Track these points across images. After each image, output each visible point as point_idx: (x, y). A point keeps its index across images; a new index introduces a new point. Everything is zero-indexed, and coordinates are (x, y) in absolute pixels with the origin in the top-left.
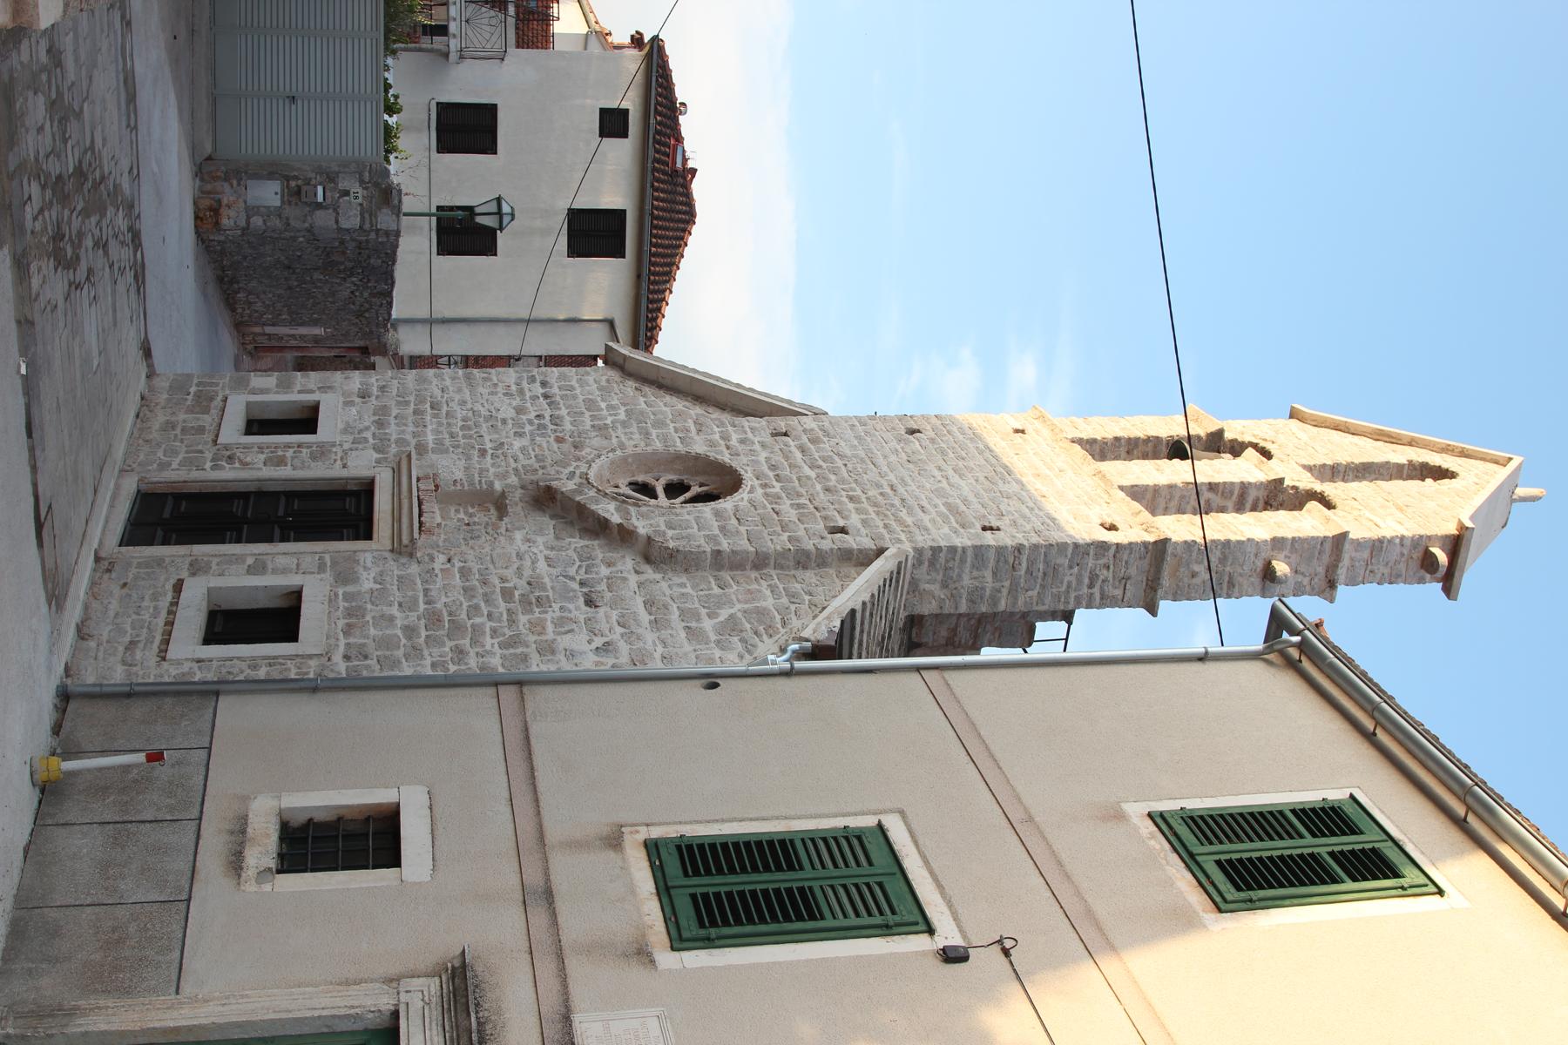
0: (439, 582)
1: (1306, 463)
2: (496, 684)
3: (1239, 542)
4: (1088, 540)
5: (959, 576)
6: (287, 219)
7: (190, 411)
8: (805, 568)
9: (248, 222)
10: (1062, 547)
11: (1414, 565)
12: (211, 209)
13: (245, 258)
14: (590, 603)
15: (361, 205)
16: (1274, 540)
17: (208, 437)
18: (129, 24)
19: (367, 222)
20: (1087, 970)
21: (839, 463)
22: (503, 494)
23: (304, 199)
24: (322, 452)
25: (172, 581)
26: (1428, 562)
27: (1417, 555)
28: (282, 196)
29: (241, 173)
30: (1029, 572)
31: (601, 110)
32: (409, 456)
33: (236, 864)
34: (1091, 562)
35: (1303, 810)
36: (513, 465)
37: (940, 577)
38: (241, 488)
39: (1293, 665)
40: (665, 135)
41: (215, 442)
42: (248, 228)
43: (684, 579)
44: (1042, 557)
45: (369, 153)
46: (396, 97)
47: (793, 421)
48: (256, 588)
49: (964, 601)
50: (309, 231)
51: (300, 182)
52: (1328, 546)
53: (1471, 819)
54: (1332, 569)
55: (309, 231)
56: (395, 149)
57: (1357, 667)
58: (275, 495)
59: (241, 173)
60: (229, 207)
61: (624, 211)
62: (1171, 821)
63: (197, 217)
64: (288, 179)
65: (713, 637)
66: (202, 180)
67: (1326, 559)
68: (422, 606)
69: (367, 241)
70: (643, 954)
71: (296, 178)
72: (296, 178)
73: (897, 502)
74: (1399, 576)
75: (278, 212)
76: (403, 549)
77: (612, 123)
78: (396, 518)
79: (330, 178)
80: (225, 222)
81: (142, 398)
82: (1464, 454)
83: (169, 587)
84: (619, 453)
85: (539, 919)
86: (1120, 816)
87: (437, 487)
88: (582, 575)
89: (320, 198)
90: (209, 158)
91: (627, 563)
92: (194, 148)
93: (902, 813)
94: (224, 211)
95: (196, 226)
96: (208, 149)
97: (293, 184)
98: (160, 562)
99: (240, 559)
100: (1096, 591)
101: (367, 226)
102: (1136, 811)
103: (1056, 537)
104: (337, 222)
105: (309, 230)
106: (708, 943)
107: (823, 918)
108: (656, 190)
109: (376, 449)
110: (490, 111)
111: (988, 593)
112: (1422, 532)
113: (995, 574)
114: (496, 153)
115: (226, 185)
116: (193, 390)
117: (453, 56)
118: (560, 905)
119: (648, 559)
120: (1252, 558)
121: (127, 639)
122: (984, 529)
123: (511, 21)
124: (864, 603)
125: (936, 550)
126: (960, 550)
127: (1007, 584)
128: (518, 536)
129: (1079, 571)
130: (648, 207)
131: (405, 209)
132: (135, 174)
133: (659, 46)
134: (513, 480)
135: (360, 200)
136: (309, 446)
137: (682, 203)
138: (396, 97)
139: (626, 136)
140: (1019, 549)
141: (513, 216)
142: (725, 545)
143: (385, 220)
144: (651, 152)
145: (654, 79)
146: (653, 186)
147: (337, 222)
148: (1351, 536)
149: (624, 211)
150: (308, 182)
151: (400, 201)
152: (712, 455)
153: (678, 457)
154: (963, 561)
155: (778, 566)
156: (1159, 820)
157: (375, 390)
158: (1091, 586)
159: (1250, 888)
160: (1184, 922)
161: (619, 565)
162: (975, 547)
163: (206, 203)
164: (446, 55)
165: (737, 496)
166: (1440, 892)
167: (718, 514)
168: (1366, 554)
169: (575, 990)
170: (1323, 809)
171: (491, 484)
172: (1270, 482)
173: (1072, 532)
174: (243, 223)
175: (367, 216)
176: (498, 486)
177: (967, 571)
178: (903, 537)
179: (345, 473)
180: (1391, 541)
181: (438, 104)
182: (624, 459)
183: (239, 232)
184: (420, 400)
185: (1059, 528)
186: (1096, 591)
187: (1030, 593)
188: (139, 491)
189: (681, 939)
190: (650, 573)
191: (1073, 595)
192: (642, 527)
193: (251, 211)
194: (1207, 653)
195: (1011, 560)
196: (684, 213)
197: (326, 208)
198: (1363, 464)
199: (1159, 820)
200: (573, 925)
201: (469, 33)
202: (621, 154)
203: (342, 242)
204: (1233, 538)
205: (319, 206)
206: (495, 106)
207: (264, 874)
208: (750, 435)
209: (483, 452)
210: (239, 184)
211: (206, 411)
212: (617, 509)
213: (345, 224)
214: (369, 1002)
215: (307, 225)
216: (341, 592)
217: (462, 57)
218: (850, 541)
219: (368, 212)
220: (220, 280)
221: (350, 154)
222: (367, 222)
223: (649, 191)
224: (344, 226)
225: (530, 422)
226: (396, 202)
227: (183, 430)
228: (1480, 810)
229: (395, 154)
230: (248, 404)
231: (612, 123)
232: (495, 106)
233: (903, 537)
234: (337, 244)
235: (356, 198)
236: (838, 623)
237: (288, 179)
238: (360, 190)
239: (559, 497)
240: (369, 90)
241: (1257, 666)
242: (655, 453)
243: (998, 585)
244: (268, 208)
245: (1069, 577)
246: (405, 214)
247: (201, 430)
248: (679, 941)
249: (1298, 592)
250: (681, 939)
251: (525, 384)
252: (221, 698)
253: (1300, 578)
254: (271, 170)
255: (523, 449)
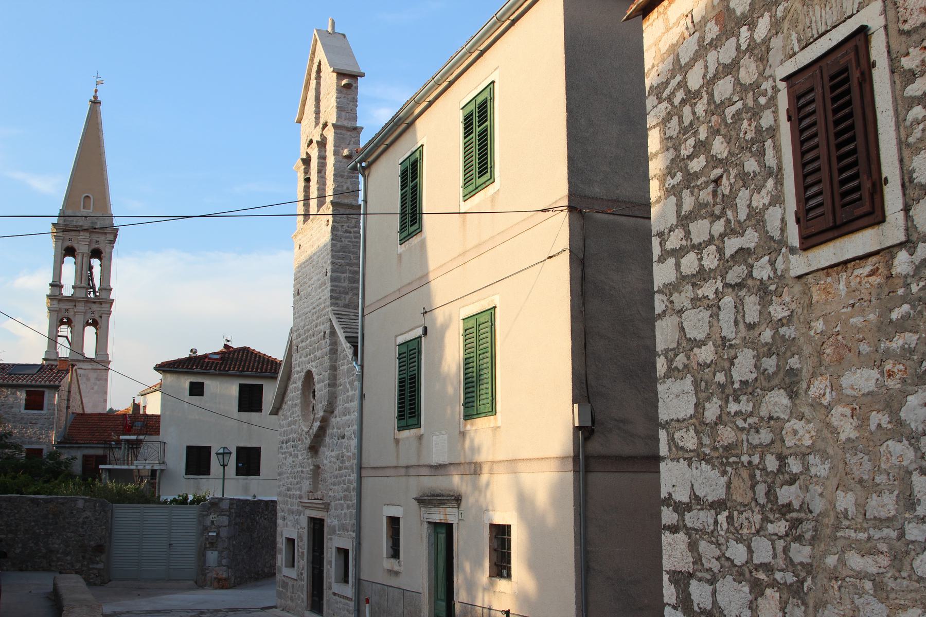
0: (336, 494)
1: (314, 126)
2: (361, 477)
3: (334, 170)
4: (330, 234)
5: (343, 287)
6: (223, 548)
7: (287, 591)
8: (337, 350)
9: (224, 566)
10: (333, 245)
11: (349, 91)
12: (219, 582)
13: (244, 568)
14: (343, 437)
15: (218, 516)
16: (334, 155)
17: (295, 583)
18: (128, 612)
19: (225, 513)
20: (432, 283)
21: (306, 328)
22: (314, 465)
23: (214, 541)
24: (300, 537)
25: (333, 595)
26: (348, 86)
27: (345, 91)
28: (213, 550)
29: (202, 568)
30: (343, 259)
31: (190, 395)
32: (301, 502)
33: (397, 573)
34: (340, 233)
35: (465, 133)
36: (306, 460)
37: (343, 296)
38: (311, 570)
39: (369, 166)
40: (203, 364)
41: (296, 580)
42: (227, 566)
43: (338, 399)
44: (337, 253)
45: (195, 512)
46: (179, 496)
47: (294, 342)
48: (335, 564)
49: (354, 285)
50: (230, 539)
51: (207, 543)
52: (339, 131)
53: (429, 99)
54: (348, 129)
55: (230, 539)
56: (204, 497)
57: (375, 137)
58: (314, 556)
59: (202, 568)
60: (217, 574)
61: (240, 384)
62: (466, 193)
63: (222, 588)
64: (205, 548)
65: (354, 392)
66: (205, 586)
67: (344, 132)
68: (342, 502)
69: (236, 513)
70: (420, 438)
71: (205, 544)
72: (205, 544)
73: (318, 308)
74: (354, 98)
75: (220, 553)
76: (327, 507)
77: (197, 390)
78: (318, 509)
79: (206, 529)
80: (225, 576)
81: (283, 610)
82: (312, 60)
83: (334, 597)
84: (300, 418)
85: (412, 471)
86: (400, 256)
87: (311, 492)
88: (336, 438)
89: (215, 534)
90: (196, 582)
91: (334, 421)
92: (190, 589)
93: (396, 336)
94: (220, 576)
95: (226, 589)
96: (192, 582)
97: (208, 546)
98: (328, 601)
99: (327, 569)
100: (352, 230)
101: (228, 513)
102: (400, 249)
103: (329, 247)
104: (225, 526)
105: (229, 539)
106: (419, 415)
107: (415, 374)
108: (229, 369)
109: (300, 515)
110: (190, 449)
111: (351, 275)
112: (335, 89)
113: (343, 273)
114: (210, 447)
115: (208, 575)
116: (281, 589)
117: (163, 467)
118: (409, 464)
119: (332, 412)
120: (342, 164)
121: (347, 612)
122: (326, 275)
123: (147, 438)
124: (344, 332)
125: (332, 297)
126: (333, 288)
127: (347, 267)
128: (325, 462)
129: (344, 237)
130: (238, 373)
131: (220, 496)
132: (192, 610)
133: (159, 367)
134: (310, 461)
135: (216, 516)
136: (298, 542)
137: (238, 354)
138: (179, 496)
139: (203, 384)
140: (332, 263)
141: (224, 448)
142: (327, 382)
143: (225, 505)
144: (211, 371)
145: (175, 370)
146: (227, 371)
147: (225, 526)
148: (334, 122)
149: (240, 384)
150: (207, 539)
151: (216, 498)
152: (302, 379)
153: (303, 393)
154: (337, 286)
155: (336, 361)
156: (403, 241)
157: (283, 514)
158: (350, 232)
159: (486, 168)
160: (423, 245)
161: (334, 423)
162: (331, 282)
163: (216, 584)
164: (162, 470)
165: (314, 373)
166: (493, 82)
167: (318, 383)
168: (343, 113)
169: (426, 463)
170: (465, 124)
171: (311, 470)
172: (318, 147)
173: (328, 239)
174: (225, 568)
175: (223, 513)
176: (312, 467)
177: (341, 284)
178: (327, 310)
179: (306, 528)
180: (337, 103)
181: (186, 474)
182: (303, 415)
183: (230, 570)
184: (286, 495)
185: (328, 243)
186: (352, 230)
187: (352, 258)
188: (311, 610)
189: (418, 424)
190: (336, 412)
191: (354, 240)
192: (321, 414)
193: (220, 564)
194: (363, 201)
195: (337, 266)
196: (243, 353)
197: (219, 531)
198: (315, 100)
199: (403, 241)
200: (413, 462)
201: (152, 459)
202: (212, 385)
203: (236, 524)
204: (333, 173)
205: (218, 534)
206: (188, 447)
207: (400, 565)
208: (297, 362)
209: (302, 472)
210: (208, 569)
211: (287, 583)
212: (316, 422)
213: (226, 523)
214: (426, 530)
215: (226, 540)
216: (338, 532)
217: (164, 463)
218: (328, 331)
219: (221, 513)
220: (256, 579)
221: (195, 520)
222: (225, 513)
223: (230, 372)
224: (227, 523)
225: (294, 451)
226: (217, 500)
227: (293, 593)
228: (383, 140)
229: (207, 497)
230: (286, 567)
231: (197, 390)
232: (188, 447)
233: (327, 310)
234: (237, 527)
235: (215, 518)
236: (348, 344)
237: (205, 548)
238: (211, 516)
239: (312, 445)
240: (166, 511)
241: (370, 180)
242: (301, 403)
243: (348, 271)
244: (218, 557)
245: (346, 242)
246: (223, 496)
247: (293, 586)
248: (418, 425)
249: (358, 143)
250: (418, 424)
251: (283, 451)
252: (362, 578)
253: (352, 142)
254: (202, 555)
255: (302, 455)
